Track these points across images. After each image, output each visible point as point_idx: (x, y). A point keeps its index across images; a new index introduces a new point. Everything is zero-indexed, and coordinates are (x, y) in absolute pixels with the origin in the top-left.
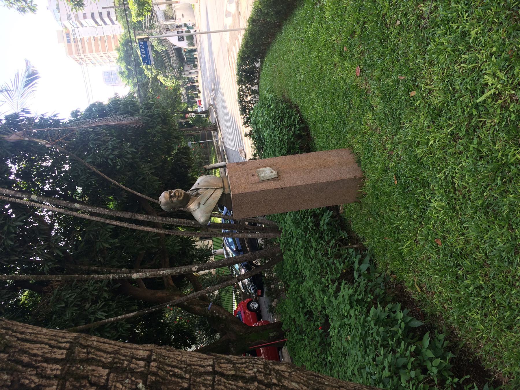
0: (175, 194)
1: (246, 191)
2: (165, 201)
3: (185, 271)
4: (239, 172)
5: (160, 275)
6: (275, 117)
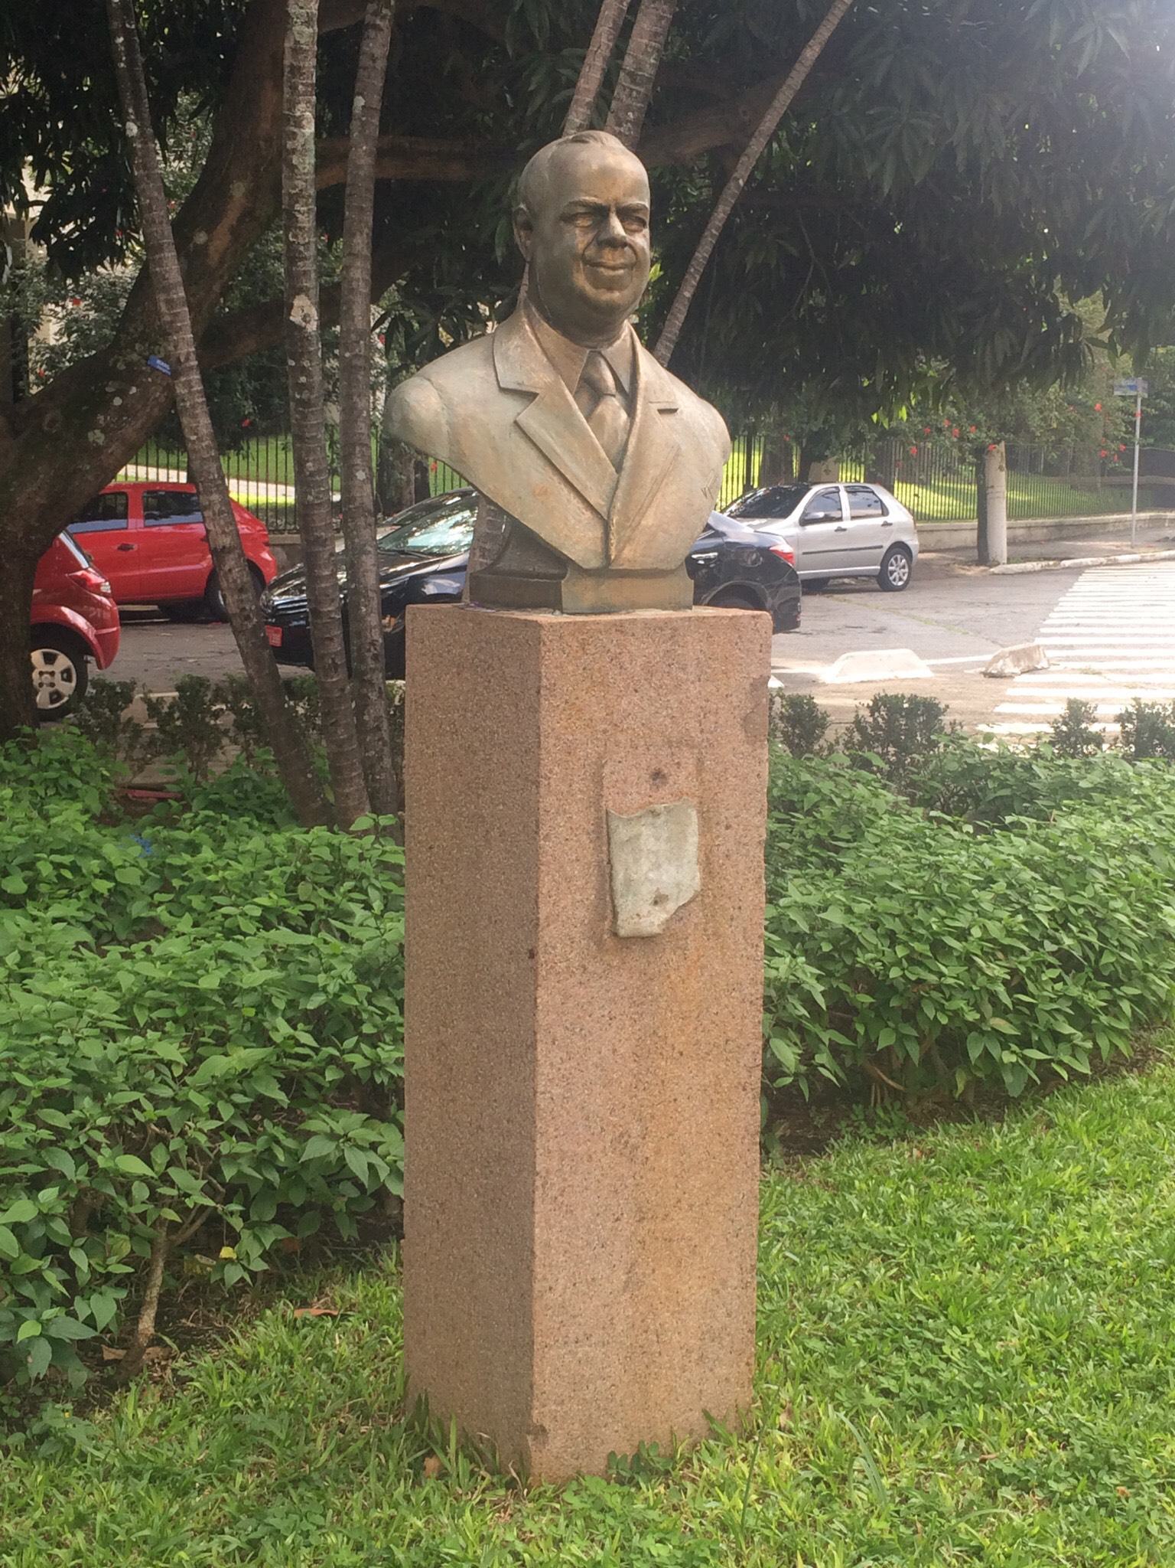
0: (616, 244)
1: (552, 720)
5: (293, 105)
6: (1100, 923)
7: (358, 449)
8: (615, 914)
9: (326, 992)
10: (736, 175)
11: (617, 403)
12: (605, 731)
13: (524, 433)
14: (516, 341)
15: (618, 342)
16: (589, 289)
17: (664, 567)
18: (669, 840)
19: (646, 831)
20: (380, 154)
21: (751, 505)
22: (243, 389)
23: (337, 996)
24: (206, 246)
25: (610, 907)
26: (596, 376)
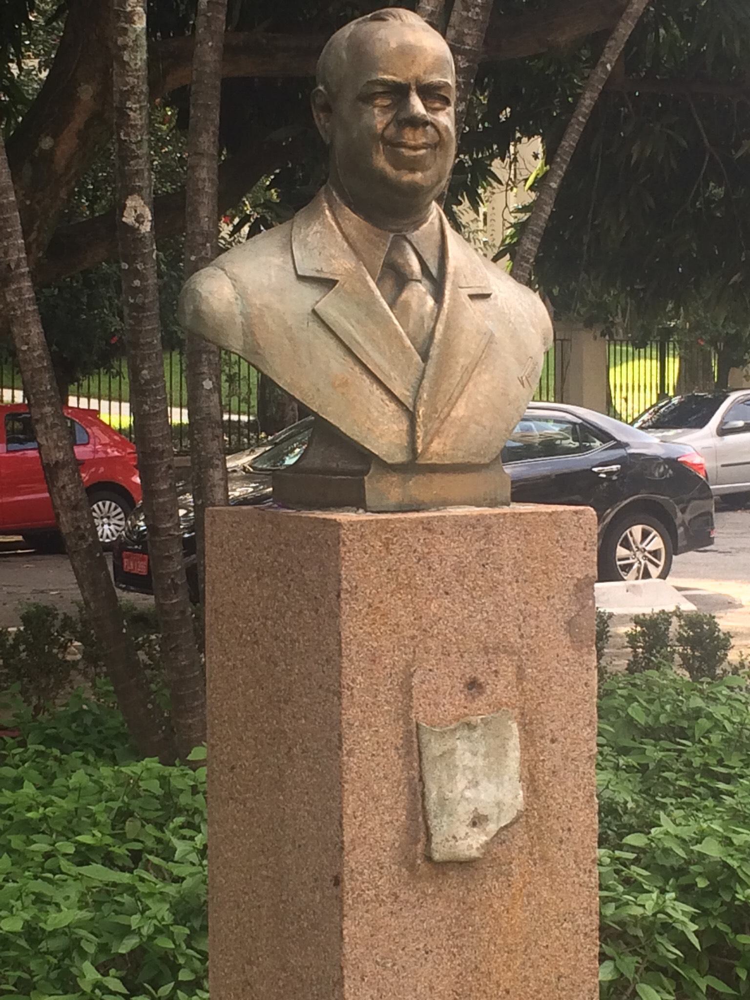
0: (417, 123)
2: (379, 50)
3: (126, 154)
4: (511, 591)
7: (204, 356)
8: (429, 837)
9: (140, 935)
10: (603, 59)
11: (424, 290)
12: (413, 638)
13: (323, 322)
14: (316, 227)
15: (425, 225)
16: (389, 169)
17: (477, 460)
18: (486, 755)
19: (461, 746)
20: (229, 51)
21: (664, 415)
22: (111, 305)
23: (151, 938)
24: (52, 150)
25: (423, 827)
26: (400, 261)
